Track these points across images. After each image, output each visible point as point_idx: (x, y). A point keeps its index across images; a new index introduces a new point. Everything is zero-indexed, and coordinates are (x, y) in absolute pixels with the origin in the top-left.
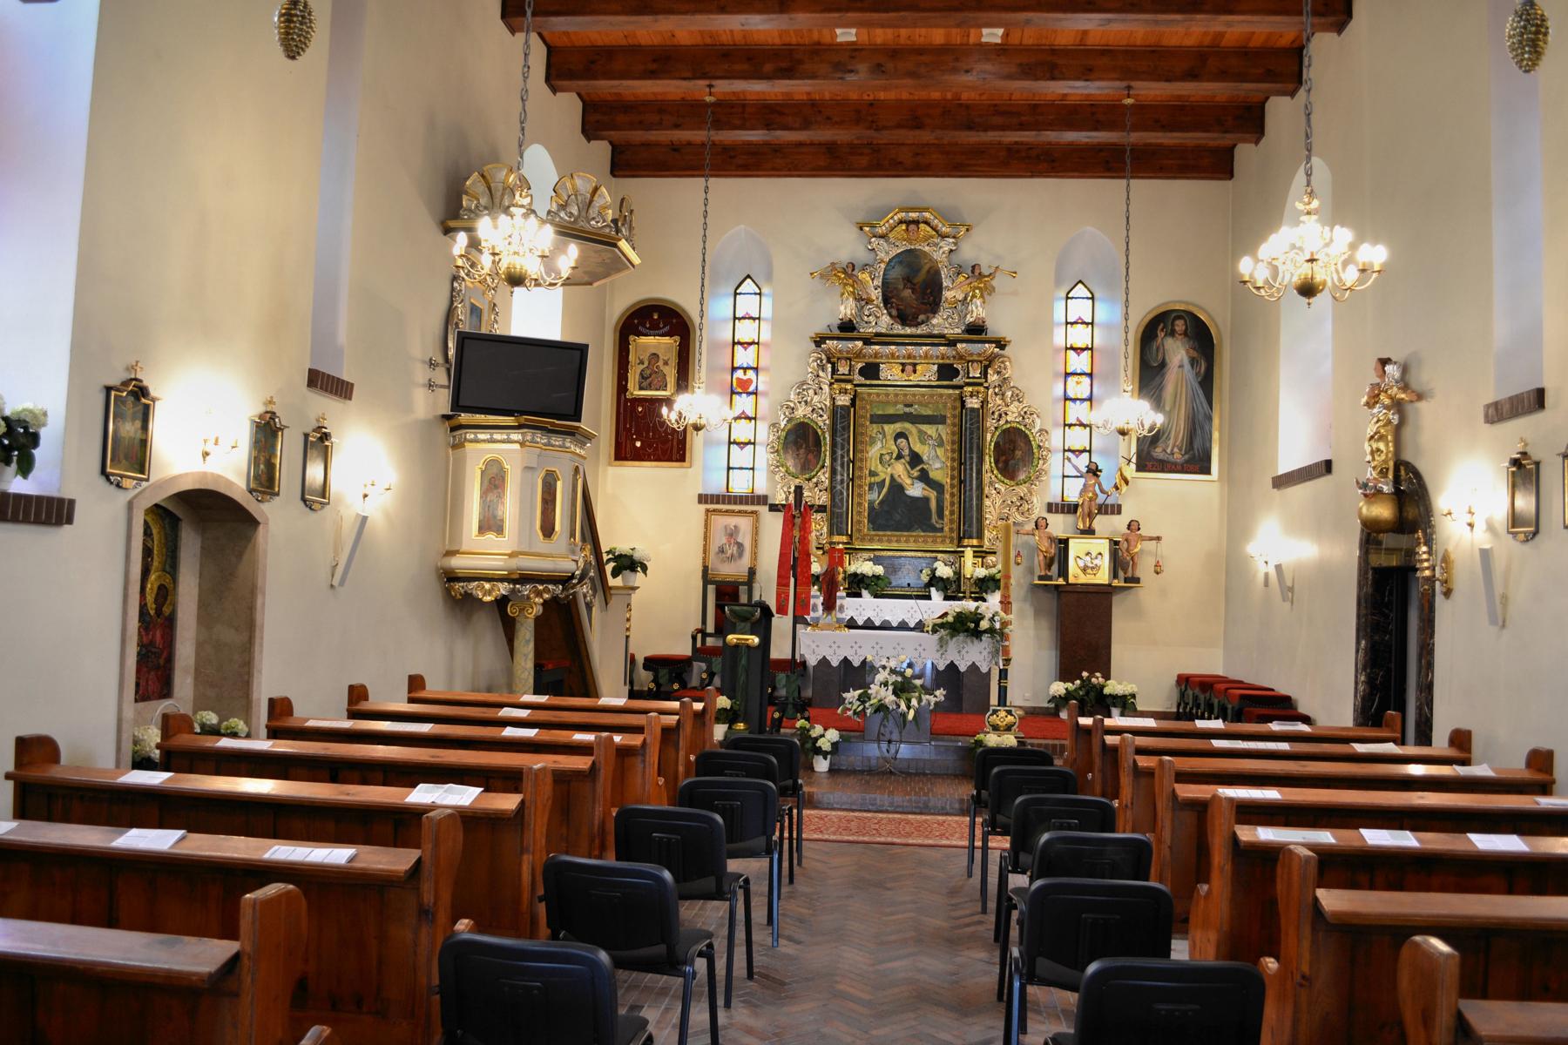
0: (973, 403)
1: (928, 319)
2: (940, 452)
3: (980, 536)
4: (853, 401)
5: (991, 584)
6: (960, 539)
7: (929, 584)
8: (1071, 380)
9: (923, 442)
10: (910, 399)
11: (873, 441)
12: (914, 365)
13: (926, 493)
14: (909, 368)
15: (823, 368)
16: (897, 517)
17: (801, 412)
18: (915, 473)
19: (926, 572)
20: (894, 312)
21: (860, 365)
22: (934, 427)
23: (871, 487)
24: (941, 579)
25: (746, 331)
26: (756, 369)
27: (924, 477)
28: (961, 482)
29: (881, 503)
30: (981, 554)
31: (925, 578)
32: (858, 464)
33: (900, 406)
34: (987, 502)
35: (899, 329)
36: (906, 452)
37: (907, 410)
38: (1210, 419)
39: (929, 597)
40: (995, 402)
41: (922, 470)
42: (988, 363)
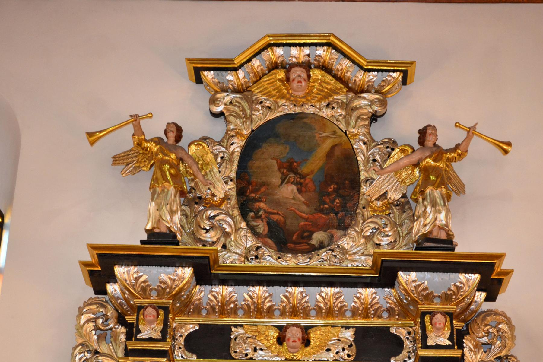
20: (262, 227)
35: (270, 260)
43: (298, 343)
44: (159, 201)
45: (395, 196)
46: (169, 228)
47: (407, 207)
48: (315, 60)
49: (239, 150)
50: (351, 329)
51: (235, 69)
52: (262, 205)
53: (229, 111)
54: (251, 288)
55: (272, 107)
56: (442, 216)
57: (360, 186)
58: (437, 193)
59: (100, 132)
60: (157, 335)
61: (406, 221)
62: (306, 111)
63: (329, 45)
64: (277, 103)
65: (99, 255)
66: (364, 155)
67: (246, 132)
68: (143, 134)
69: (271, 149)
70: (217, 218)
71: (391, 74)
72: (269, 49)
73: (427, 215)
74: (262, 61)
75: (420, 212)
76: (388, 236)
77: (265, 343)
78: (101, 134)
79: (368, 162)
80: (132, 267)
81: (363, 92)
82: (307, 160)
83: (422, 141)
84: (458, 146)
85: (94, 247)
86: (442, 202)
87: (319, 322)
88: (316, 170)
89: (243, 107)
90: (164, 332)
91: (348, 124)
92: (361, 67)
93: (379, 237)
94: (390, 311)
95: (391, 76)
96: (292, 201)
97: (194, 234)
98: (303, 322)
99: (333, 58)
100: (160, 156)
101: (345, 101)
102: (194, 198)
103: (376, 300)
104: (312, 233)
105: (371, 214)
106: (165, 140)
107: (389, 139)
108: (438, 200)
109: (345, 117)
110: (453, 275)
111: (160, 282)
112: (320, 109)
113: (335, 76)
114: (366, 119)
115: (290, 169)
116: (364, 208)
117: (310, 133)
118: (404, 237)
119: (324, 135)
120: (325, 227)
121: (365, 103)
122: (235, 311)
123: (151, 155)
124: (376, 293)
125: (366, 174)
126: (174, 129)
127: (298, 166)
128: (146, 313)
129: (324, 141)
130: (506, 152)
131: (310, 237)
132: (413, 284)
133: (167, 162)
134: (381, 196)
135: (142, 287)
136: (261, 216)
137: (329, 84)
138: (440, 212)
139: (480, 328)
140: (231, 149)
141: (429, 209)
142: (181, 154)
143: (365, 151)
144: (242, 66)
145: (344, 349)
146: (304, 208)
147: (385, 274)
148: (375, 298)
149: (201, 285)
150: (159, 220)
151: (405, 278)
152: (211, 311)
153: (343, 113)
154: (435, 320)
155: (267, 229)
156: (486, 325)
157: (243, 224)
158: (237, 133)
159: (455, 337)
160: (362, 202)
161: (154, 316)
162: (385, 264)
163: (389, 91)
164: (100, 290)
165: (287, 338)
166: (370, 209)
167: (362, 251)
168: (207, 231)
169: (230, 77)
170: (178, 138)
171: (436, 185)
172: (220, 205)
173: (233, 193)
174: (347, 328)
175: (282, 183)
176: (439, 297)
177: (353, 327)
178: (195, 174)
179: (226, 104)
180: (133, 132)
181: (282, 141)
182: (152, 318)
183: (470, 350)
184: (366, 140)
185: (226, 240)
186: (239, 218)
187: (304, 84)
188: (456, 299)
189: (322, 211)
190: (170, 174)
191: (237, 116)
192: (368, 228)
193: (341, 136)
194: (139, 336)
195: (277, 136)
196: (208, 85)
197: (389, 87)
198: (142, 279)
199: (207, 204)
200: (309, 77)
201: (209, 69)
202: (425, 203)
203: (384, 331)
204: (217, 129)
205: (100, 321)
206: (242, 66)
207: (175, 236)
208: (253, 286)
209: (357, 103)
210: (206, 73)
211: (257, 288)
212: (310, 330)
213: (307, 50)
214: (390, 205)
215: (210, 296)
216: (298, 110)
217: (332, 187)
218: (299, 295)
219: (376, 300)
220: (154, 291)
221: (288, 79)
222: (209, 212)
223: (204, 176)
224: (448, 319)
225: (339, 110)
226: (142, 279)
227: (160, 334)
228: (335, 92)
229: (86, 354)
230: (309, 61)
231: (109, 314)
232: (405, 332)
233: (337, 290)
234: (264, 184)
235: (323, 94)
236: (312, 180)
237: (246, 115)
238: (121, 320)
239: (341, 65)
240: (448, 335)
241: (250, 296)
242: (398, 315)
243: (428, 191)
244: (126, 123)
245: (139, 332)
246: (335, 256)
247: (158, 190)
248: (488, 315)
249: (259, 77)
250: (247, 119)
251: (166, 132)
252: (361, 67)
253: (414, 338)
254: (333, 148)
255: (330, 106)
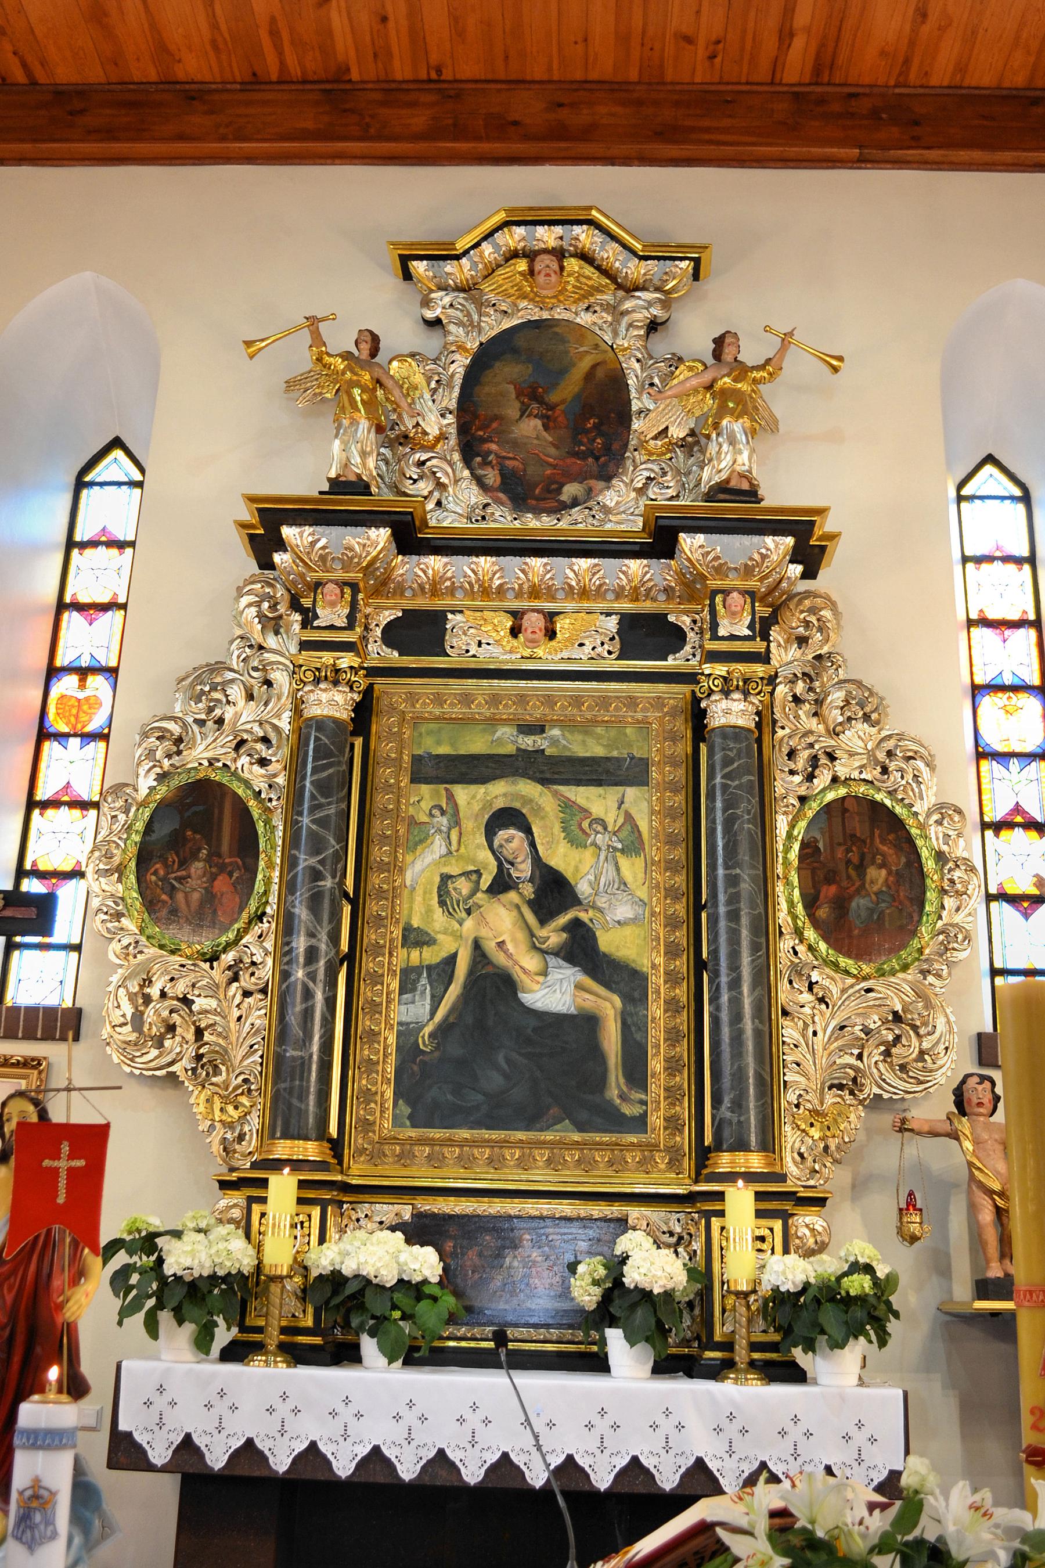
0: (729, 712)
1: (589, 492)
2: (631, 868)
3: (769, 1144)
4: (364, 711)
5: (829, 1317)
6: (703, 1155)
7: (604, 1314)
8: (989, 703)
9: (576, 841)
10: (536, 712)
11: (417, 836)
12: (551, 617)
13: (588, 1002)
14: (534, 622)
15: (273, 624)
16: (493, 1081)
17: (201, 752)
18: (553, 935)
19: (591, 1268)
20: (492, 477)
21: (387, 616)
22: (613, 793)
23: (408, 984)
24: (645, 1295)
25: (96, 576)
26: (112, 672)
27: (581, 949)
28: (700, 965)
29: (443, 1031)
30: (778, 1202)
31: (586, 1293)
32: (373, 907)
33: (505, 732)
34: (790, 1032)
35: (503, 520)
36: (524, 869)
37: (528, 742)
38: (986, 1048)
39: (597, 1363)
40: (796, 725)
41: (576, 925)
42: (771, 610)
43: (540, 635)
44: (346, 438)
45: (677, 432)
46: (359, 476)
47: (695, 449)
48: (571, 245)
49: (461, 371)
50: (614, 617)
51: (457, 257)
52: (494, 447)
53: (448, 316)
54: (474, 559)
55: (510, 311)
56: (744, 458)
57: (631, 420)
58: (737, 426)
59: (263, 340)
60: (342, 622)
61: (694, 468)
62: (557, 317)
63: (591, 223)
64: (515, 305)
65: (259, 510)
66: (637, 377)
67: (473, 345)
68: (325, 344)
69: (506, 369)
70: (428, 464)
71: (677, 263)
72: (506, 229)
73: (723, 456)
74: (497, 247)
75: (713, 453)
76: (668, 487)
77: (494, 634)
78: (264, 344)
79: (643, 386)
80: (307, 527)
81: (637, 289)
82: (557, 384)
83: (717, 355)
84: (768, 361)
85: (252, 499)
86: (744, 437)
87: (570, 605)
88: (569, 399)
89: (468, 311)
90: (351, 618)
91: (615, 334)
92: (634, 253)
93: (655, 489)
94: (668, 591)
95: (677, 266)
96: (535, 442)
97: (396, 487)
98: (549, 606)
99: (596, 243)
100: (348, 375)
101: (612, 302)
102: (398, 437)
103: (648, 576)
104: (562, 486)
105: (646, 457)
106: (356, 353)
107: (673, 354)
108: (738, 435)
109: (611, 324)
110: (756, 539)
111: (346, 549)
112: (576, 314)
113: (598, 268)
114: (641, 327)
115: (532, 396)
116: (635, 450)
117: (561, 347)
118: (690, 491)
119: (582, 349)
120: (580, 477)
121: (641, 307)
122: (452, 591)
123: (334, 376)
124: (649, 566)
125: (639, 403)
126: (369, 338)
127: (545, 392)
128: (325, 590)
129: (581, 359)
130: (835, 370)
131: (559, 491)
132: (700, 551)
133: (357, 384)
134: (660, 433)
135: (321, 555)
136: (491, 462)
137: (590, 278)
138: (740, 452)
139: (793, 615)
140: (451, 370)
141: (725, 447)
142: (378, 373)
143: (639, 372)
144: (466, 252)
145: (603, 644)
146: (552, 451)
147: (660, 540)
148: (647, 573)
149: (404, 555)
150: (346, 465)
151: (690, 543)
152: (419, 592)
153: (610, 319)
154: (729, 600)
155: (499, 480)
156: (802, 612)
157: (466, 473)
158: (459, 347)
159: (757, 626)
160: (633, 443)
161: (336, 595)
162: (661, 522)
163: (673, 290)
164: (266, 564)
165: (523, 628)
166: (643, 452)
167: (632, 510)
168: (415, 481)
169: (449, 267)
170: (374, 352)
171: (736, 414)
172: (434, 446)
173: (453, 430)
174: (608, 615)
175: (521, 416)
176: (735, 569)
177: (616, 614)
178: (398, 401)
179: (444, 308)
180: (310, 342)
181: (523, 358)
182: (334, 597)
183: (779, 645)
184: (640, 356)
185: (441, 495)
186: (460, 465)
187: (554, 278)
188: (760, 572)
189: (576, 455)
190: (362, 400)
191: (460, 324)
192: (640, 478)
193: (606, 352)
194: (315, 624)
195: (515, 351)
196: (420, 281)
197: (674, 282)
198: (319, 545)
199: (415, 445)
200: (562, 268)
201: (421, 258)
202: (720, 440)
203: (660, 619)
204: (430, 343)
205: (266, 605)
206: (466, 252)
207: (367, 486)
208: (477, 556)
209: (628, 305)
210: (415, 263)
211: (482, 559)
212: (557, 618)
213: (559, 230)
214: (671, 446)
215: (417, 570)
216: (546, 315)
217: (592, 421)
218: (542, 569)
219: (648, 576)
220: (337, 561)
221: (532, 272)
222: (417, 456)
223: (410, 405)
224: (749, 600)
225: (604, 315)
226: (319, 545)
227: (345, 620)
228: (598, 290)
229: (247, 649)
230: (561, 246)
231: (279, 595)
232: (687, 620)
233: (596, 561)
234: (496, 418)
235: (582, 292)
236: (563, 412)
237: (472, 322)
238: (295, 605)
239: (607, 252)
240: (747, 622)
241: (473, 571)
242: (679, 597)
243: (724, 422)
244: (299, 328)
245: (316, 617)
246: (594, 516)
247: (346, 422)
248: (806, 598)
249: (490, 272)
250: (473, 327)
251: (357, 343)
252: (634, 253)
253: (701, 628)
254: (594, 367)
255: (591, 310)
